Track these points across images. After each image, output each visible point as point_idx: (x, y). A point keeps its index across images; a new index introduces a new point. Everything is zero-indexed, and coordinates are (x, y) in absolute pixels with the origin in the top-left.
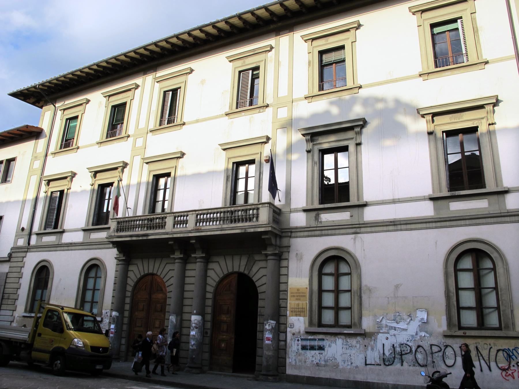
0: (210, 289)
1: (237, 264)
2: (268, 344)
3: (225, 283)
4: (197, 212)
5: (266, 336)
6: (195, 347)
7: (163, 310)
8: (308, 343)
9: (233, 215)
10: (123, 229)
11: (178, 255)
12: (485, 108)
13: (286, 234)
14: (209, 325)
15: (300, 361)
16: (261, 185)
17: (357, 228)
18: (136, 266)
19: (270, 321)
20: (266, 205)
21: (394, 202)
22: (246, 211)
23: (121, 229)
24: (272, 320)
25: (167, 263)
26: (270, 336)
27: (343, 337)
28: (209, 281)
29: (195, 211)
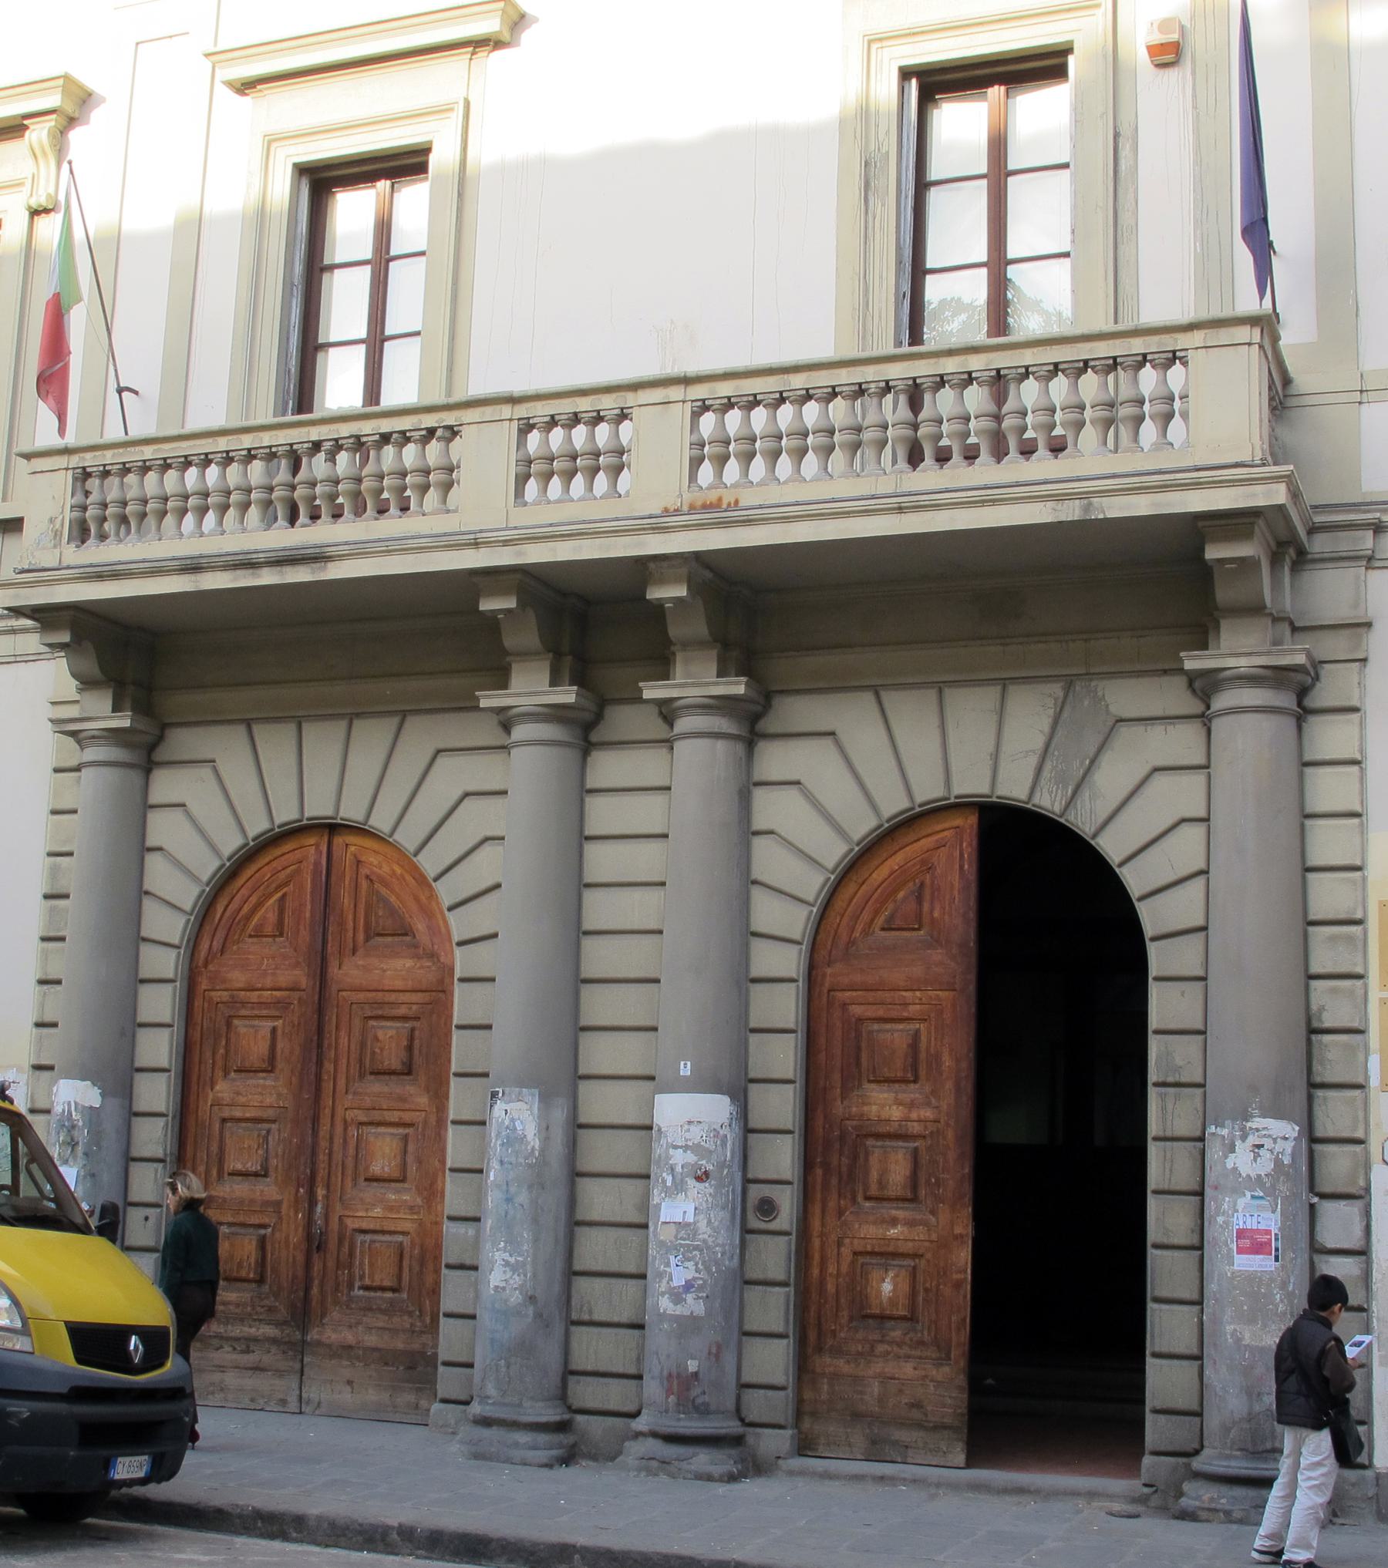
0: (774, 915)
1: (990, 745)
2: (1251, 1278)
3: (883, 872)
4: (699, 392)
5: (1239, 1222)
6: (694, 1305)
7: (424, 1059)
9: (370, 468)
11: (532, 687)
13: (1344, 543)
14: (781, 1157)
16: (1125, 218)
18: (206, 772)
19: (1257, 1122)
20: (1243, 333)
22: (999, 383)
23: (356, 496)
24: (1278, 1115)
25: (439, 751)
26: (1270, 1221)
28: (159, 874)
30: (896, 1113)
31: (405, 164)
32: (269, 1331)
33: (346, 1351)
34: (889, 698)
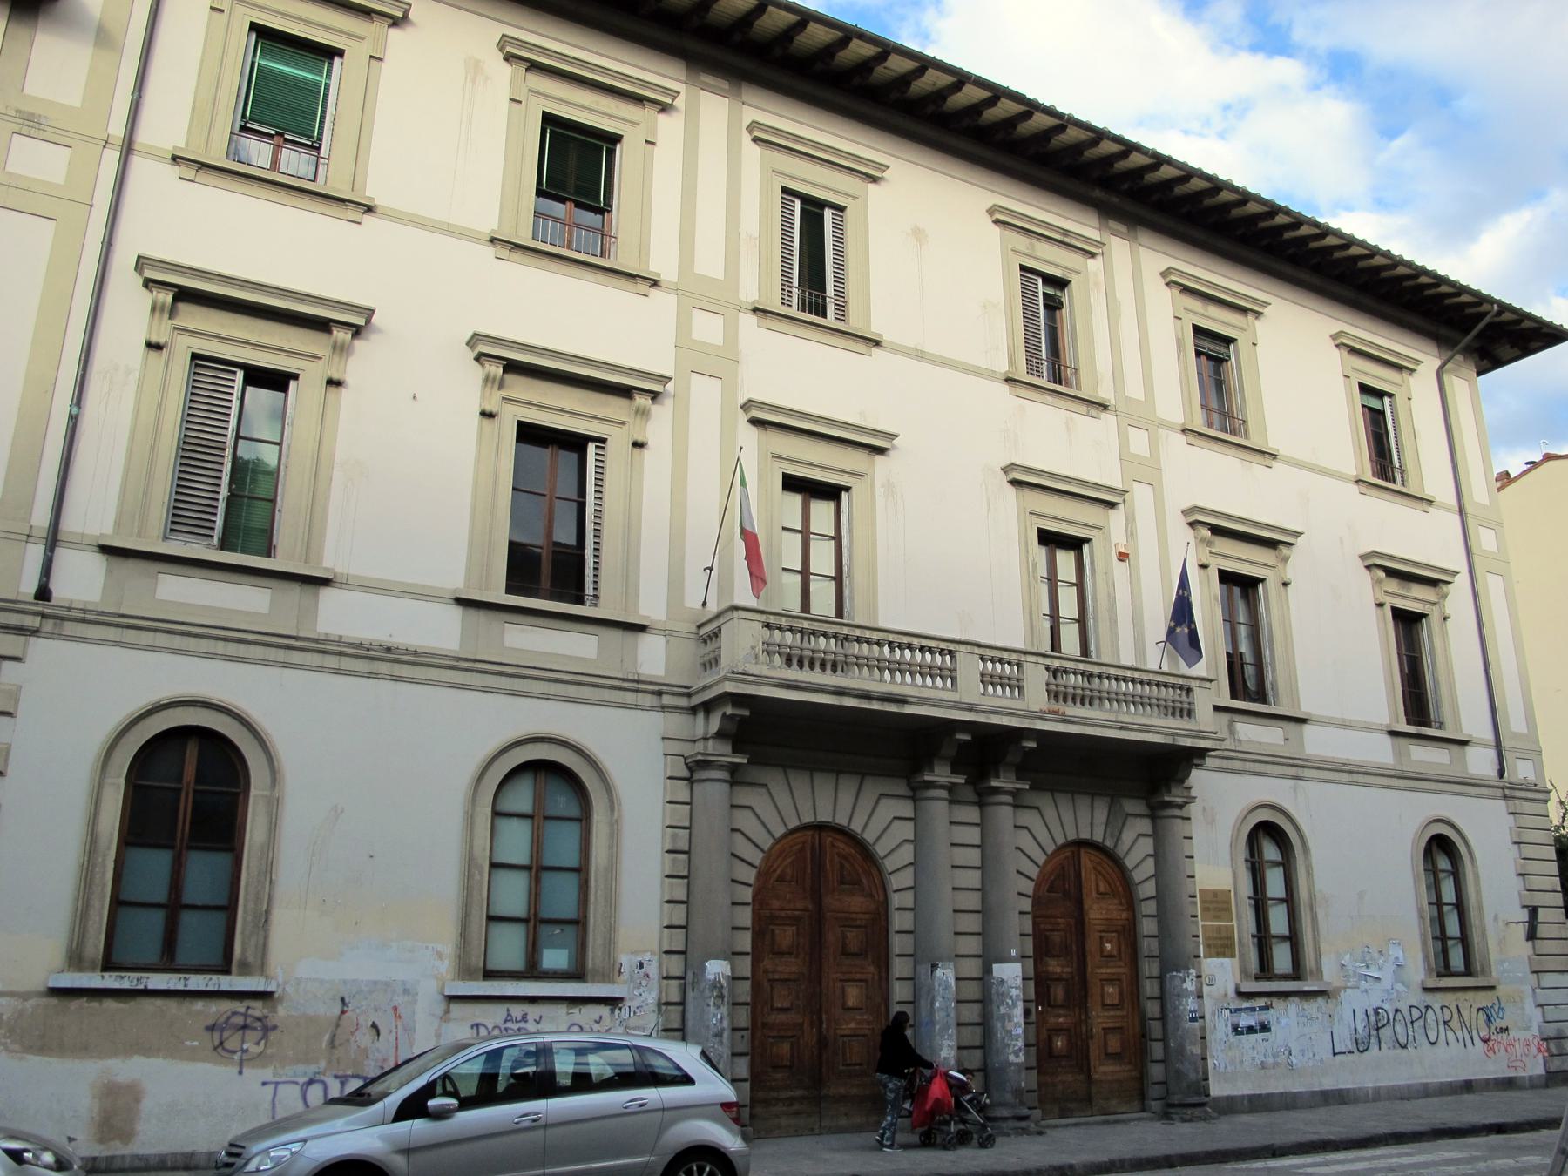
8: (1246, 1020)
10: (1181, 710)
12: (329, 331)
15: (1233, 1066)
17: (1298, 767)
21: (1344, 725)
27: (1297, 999)
29: (979, 645)
30: (1058, 970)
31: (831, 493)
32: (799, 1093)
33: (842, 1099)
34: (1057, 795)
